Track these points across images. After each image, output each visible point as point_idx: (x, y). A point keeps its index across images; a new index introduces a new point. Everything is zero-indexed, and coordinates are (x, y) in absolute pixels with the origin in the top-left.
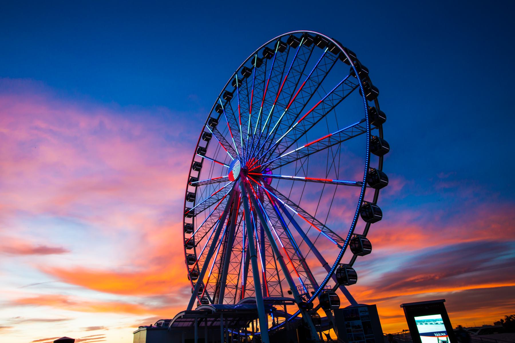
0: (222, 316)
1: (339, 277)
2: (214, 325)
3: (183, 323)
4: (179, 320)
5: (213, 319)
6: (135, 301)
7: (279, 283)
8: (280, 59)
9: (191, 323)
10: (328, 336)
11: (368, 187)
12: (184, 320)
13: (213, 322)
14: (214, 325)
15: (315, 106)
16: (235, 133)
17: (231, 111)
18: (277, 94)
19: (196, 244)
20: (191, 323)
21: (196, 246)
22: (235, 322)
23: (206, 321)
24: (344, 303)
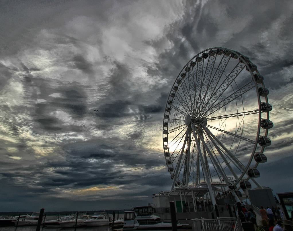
0: (192, 191)
1: (256, 159)
2: (187, 195)
3: (174, 194)
4: (173, 192)
5: (187, 192)
6: (284, 135)
7: (262, 142)
8: (200, 64)
9: (177, 194)
10: (246, 203)
11: (262, 112)
12: (175, 192)
13: (187, 193)
14: (187, 195)
15: (215, 73)
16: (222, 126)
17: (178, 97)
18: (212, 95)
19: (172, 162)
20: (177, 194)
21: (172, 163)
22: (197, 194)
23: (184, 193)
24: (254, 187)
